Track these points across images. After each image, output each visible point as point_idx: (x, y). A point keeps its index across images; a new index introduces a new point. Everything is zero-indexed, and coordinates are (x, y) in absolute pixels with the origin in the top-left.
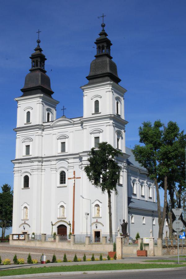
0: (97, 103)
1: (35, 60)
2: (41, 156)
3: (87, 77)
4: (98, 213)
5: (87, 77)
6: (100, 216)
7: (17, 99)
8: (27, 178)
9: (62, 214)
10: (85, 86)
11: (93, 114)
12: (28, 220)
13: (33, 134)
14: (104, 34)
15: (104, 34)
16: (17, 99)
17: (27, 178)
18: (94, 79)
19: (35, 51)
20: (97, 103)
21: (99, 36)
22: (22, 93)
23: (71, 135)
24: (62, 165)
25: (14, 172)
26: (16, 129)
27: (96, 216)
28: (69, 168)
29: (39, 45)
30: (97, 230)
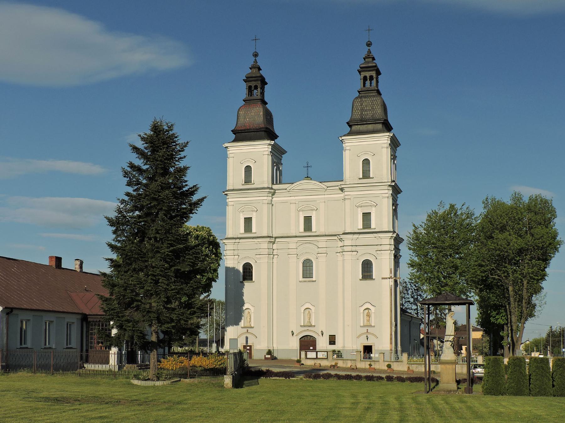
0: (366, 162)
1: (253, 84)
2: (266, 235)
3: (232, 131)
4: (368, 321)
5: (232, 131)
6: (313, 324)
7: (227, 145)
8: (308, 265)
9: (307, 320)
10: (345, 136)
11: (360, 179)
12: (251, 327)
13: (259, 201)
14: (369, 57)
15: (369, 57)
16: (227, 145)
17: (308, 265)
18: (358, 126)
19: (250, 71)
20: (366, 162)
21: (363, 61)
22: (234, 136)
23: (322, 206)
24: (309, 250)
25: (227, 257)
26: (227, 191)
27: (365, 324)
28: (319, 255)
29: (256, 60)
30: (368, 343)
